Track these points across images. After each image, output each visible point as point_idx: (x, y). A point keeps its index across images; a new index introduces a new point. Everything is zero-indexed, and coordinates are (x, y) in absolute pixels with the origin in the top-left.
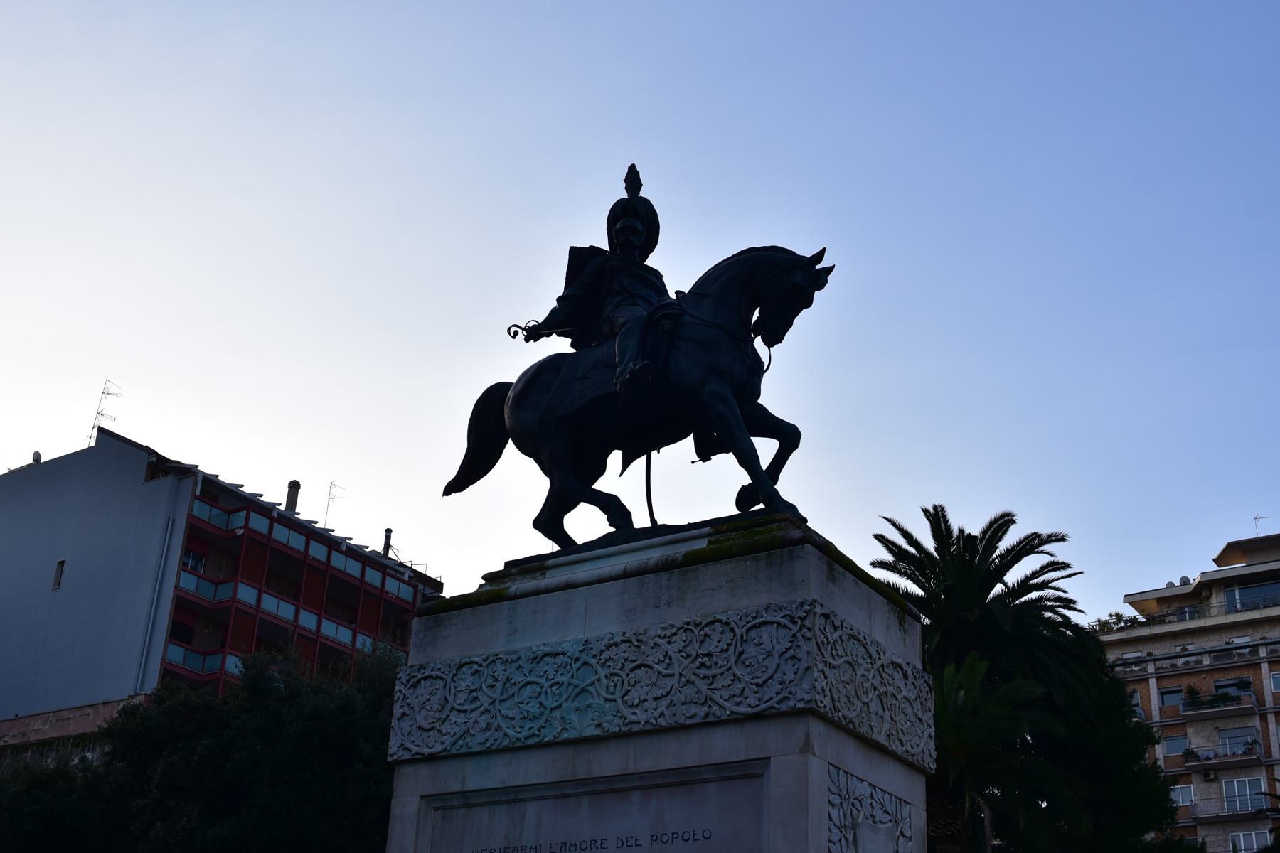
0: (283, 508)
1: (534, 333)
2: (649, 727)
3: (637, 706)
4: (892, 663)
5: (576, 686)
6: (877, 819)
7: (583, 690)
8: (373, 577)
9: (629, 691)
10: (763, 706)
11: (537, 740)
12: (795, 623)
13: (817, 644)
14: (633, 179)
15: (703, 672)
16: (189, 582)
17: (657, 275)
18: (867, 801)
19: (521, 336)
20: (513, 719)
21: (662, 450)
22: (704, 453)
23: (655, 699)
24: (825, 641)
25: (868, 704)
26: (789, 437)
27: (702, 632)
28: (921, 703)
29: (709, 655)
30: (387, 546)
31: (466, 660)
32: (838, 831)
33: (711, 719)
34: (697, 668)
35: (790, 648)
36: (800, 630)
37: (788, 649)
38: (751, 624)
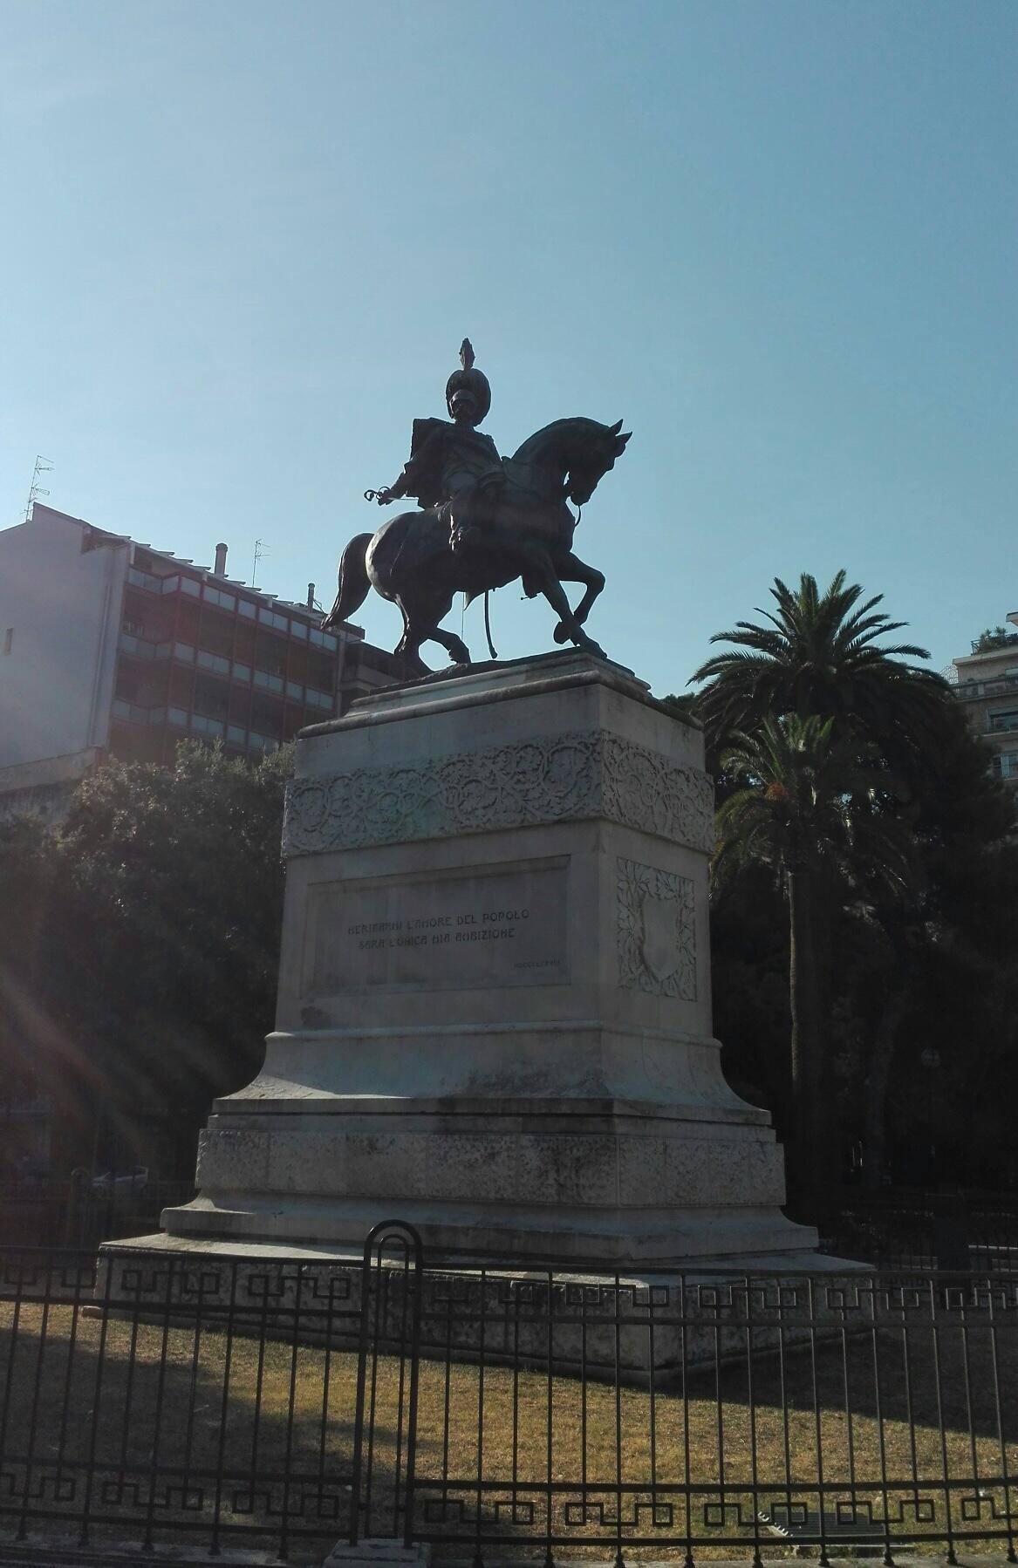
0: (212, 571)
1: (386, 498)
2: (480, 830)
3: (470, 813)
4: (675, 770)
5: (424, 797)
6: (662, 896)
7: (430, 800)
8: (298, 630)
9: (464, 801)
10: (564, 815)
11: (395, 840)
12: (587, 748)
13: (605, 765)
14: (467, 352)
15: (519, 787)
16: (130, 644)
17: (488, 440)
18: (652, 885)
19: (375, 499)
20: (377, 823)
21: (609, 423)
22: (531, 593)
23: (484, 808)
24: (613, 761)
25: (652, 807)
26: (595, 582)
27: (518, 755)
28: (703, 800)
29: (524, 773)
30: (311, 599)
31: (340, 775)
32: (626, 910)
33: (526, 824)
34: (515, 783)
35: (584, 769)
36: (592, 754)
37: (583, 769)
38: (555, 748)
